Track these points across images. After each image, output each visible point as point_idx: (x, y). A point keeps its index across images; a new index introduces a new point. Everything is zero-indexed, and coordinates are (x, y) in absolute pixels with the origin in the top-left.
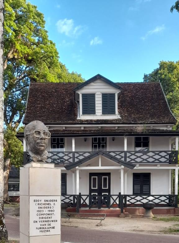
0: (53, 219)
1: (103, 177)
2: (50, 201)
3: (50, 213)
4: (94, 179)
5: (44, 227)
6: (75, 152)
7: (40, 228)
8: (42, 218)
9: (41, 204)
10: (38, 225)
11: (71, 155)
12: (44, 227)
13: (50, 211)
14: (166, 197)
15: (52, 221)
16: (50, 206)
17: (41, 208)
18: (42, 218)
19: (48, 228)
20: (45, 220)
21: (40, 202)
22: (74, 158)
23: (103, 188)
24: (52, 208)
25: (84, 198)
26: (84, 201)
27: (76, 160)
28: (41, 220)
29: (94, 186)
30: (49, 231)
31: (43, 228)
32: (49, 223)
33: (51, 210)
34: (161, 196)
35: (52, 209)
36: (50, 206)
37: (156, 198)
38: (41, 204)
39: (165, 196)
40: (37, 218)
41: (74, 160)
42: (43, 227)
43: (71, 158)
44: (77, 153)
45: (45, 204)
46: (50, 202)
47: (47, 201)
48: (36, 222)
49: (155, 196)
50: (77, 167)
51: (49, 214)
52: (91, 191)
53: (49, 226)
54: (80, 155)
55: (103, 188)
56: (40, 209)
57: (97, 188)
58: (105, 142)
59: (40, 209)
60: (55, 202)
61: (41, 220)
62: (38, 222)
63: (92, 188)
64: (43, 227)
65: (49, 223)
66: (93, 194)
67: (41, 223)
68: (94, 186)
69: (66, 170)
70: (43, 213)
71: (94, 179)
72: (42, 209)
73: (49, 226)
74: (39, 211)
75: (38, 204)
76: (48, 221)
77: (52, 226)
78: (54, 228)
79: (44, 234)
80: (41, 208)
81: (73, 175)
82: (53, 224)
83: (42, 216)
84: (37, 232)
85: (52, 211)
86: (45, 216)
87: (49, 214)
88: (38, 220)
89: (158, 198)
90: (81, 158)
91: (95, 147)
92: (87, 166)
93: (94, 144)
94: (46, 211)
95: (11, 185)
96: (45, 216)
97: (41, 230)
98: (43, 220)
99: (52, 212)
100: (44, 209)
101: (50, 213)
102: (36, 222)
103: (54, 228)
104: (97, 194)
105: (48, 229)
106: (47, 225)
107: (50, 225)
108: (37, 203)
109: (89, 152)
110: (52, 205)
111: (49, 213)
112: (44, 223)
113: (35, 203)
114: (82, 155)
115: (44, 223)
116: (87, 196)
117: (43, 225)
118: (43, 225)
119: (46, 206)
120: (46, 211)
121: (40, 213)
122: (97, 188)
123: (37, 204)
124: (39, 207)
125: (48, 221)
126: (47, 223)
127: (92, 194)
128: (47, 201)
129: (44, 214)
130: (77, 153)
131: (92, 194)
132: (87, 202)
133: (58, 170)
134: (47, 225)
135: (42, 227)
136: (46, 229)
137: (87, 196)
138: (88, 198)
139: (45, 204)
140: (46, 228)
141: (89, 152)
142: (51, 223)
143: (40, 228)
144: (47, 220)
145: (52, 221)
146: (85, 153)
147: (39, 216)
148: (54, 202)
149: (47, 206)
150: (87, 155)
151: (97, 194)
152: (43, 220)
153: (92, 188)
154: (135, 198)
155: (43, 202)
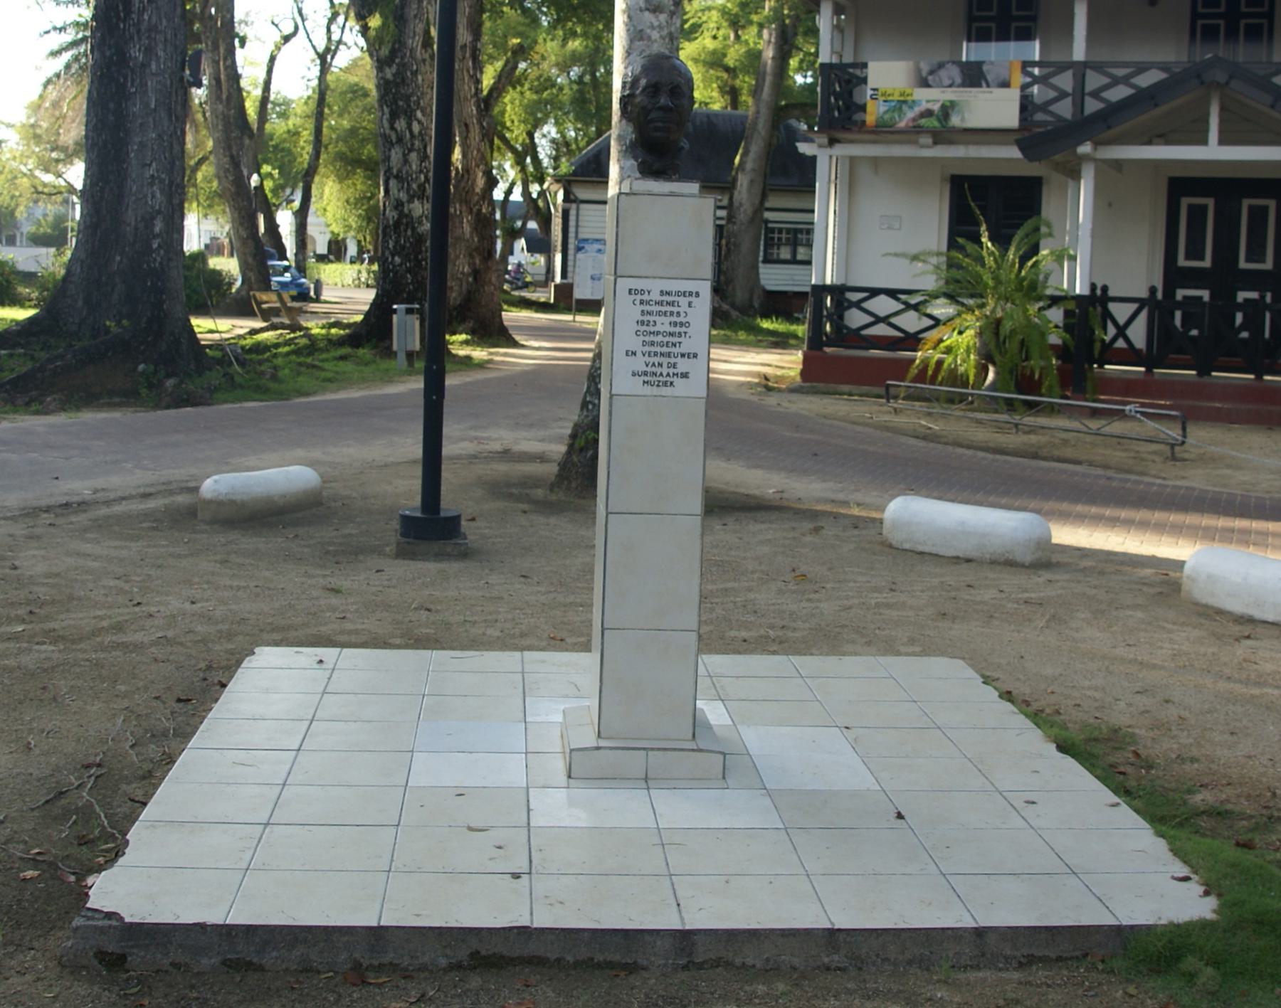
0: (683, 349)
1: (1246, 203)
2: (678, 294)
3: (678, 329)
4: (1197, 215)
5: (659, 370)
6: (1085, 65)
7: (645, 374)
8: (652, 344)
9: (648, 303)
10: (639, 364)
11: (1065, 81)
12: (659, 370)
13: (675, 324)
14: (898, 299)
15: (683, 355)
16: (675, 309)
17: (649, 313)
18: (652, 344)
19: (668, 375)
20: (658, 349)
21: (646, 297)
22: (1079, 94)
23: (1243, 265)
24: (683, 315)
25: (1120, 312)
26: (1121, 331)
27: (1092, 106)
28: (647, 349)
29: (1195, 251)
30: (671, 383)
31: (654, 374)
32: (672, 360)
33: (678, 320)
34: (874, 292)
35: (682, 319)
36: (675, 309)
37: (909, 307)
38: (648, 303)
39: (893, 293)
40: (636, 344)
41: (1079, 105)
42: (654, 369)
43: (1063, 95)
44: (1099, 67)
45: (660, 303)
46: (676, 299)
47: (668, 293)
48: (634, 354)
49: (903, 297)
50: (1085, 149)
51: (671, 334)
52: (1174, 276)
53: (671, 371)
54: (1115, 82)
55: (1243, 265)
56: (646, 318)
57: (1207, 263)
58: (1200, 22)
59: (646, 318)
60: (692, 299)
61: (647, 349)
62: (639, 354)
63: (1182, 262)
64: (654, 369)
65: (672, 360)
66: (1185, 297)
67: (647, 358)
68: (1195, 251)
69: (1026, 161)
70: (656, 329)
71: (1197, 215)
72: (651, 318)
73: (671, 371)
74: (643, 323)
75: (642, 302)
76: (669, 355)
77: (680, 369)
78: (685, 375)
79: (655, 391)
80: (649, 313)
81: (1071, 183)
82: (683, 364)
83: (652, 338)
84: (636, 386)
85: (682, 324)
86: (659, 338)
87: (671, 334)
88: (639, 349)
89: (916, 307)
90: (1118, 94)
91: (1210, 34)
92: (1149, 143)
93: (1200, 22)
94: (663, 324)
95: (780, 231)
96: (659, 338)
97: (646, 379)
98: (653, 349)
99: (684, 329)
100: (657, 319)
101: (678, 329)
102: (634, 354)
103: (685, 375)
104: (1205, 295)
105: (668, 379)
106: (665, 365)
107: (674, 366)
108: (639, 297)
109: (1163, 67)
110: (684, 307)
111: (672, 329)
112: (656, 360)
113: (633, 297)
114: (1125, 80)
115: (656, 360)
116: (1134, 306)
117: (654, 365)
118: (654, 365)
119: (664, 309)
120: (663, 324)
121: (645, 328)
122: (1207, 263)
123: (637, 302)
124: (643, 311)
125: (669, 355)
126: (665, 361)
127: (1180, 294)
128: (668, 293)
129: (658, 333)
130: (1099, 67)
131: (1180, 294)
132: (1138, 334)
133: (706, 200)
134: (665, 365)
135: (649, 369)
136: (661, 379)
137: (1134, 306)
138: (1143, 316)
139: (660, 303)
140: (661, 374)
141: (1163, 67)
142: (679, 360)
143: (645, 374)
144: (665, 350)
145: (683, 355)
146: (1141, 68)
147: (642, 338)
148: (690, 299)
149: (669, 309)
150: (1146, 80)
151: (1205, 295)
152: (653, 349)
153: (1182, 262)
154: (865, 305)
155: (656, 296)
